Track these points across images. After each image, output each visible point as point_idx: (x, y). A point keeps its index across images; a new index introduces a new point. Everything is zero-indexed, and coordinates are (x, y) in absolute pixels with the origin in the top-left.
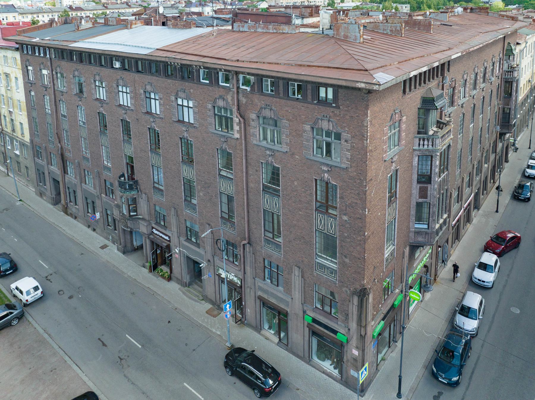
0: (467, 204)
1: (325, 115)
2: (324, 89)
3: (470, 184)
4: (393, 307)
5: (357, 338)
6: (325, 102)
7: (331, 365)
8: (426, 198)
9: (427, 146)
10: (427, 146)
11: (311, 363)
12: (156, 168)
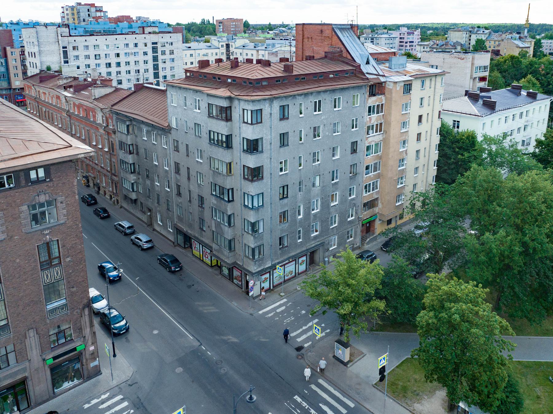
1: (41, 191)
2: (35, 171)
6: (38, 181)
7: (69, 383)
11: (57, 394)
12: (217, 160)
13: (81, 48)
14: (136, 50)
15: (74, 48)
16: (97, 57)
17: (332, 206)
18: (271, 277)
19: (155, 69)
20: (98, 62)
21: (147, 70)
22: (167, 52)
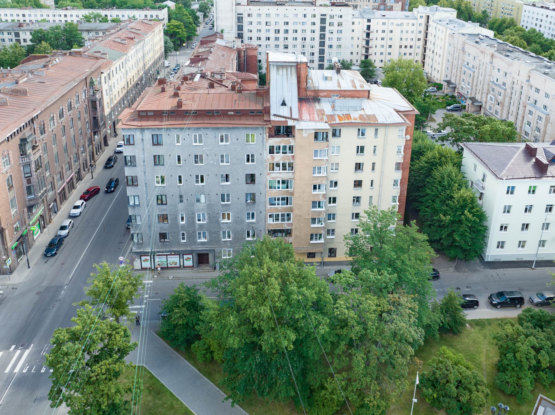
0: (68, 179)
3: (70, 168)
4: (22, 236)
5: (4, 251)
8: (31, 183)
9: (26, 160)
10: (26, 160)
13: (254, 15)
14: (304, 20)
15: (249, 15)
16: (268, 24)
17: (223, 223)
18: (152, 260)
19: (321, 38)
20: (268, 28)
21: (314, 38)
22: (336, 24)
